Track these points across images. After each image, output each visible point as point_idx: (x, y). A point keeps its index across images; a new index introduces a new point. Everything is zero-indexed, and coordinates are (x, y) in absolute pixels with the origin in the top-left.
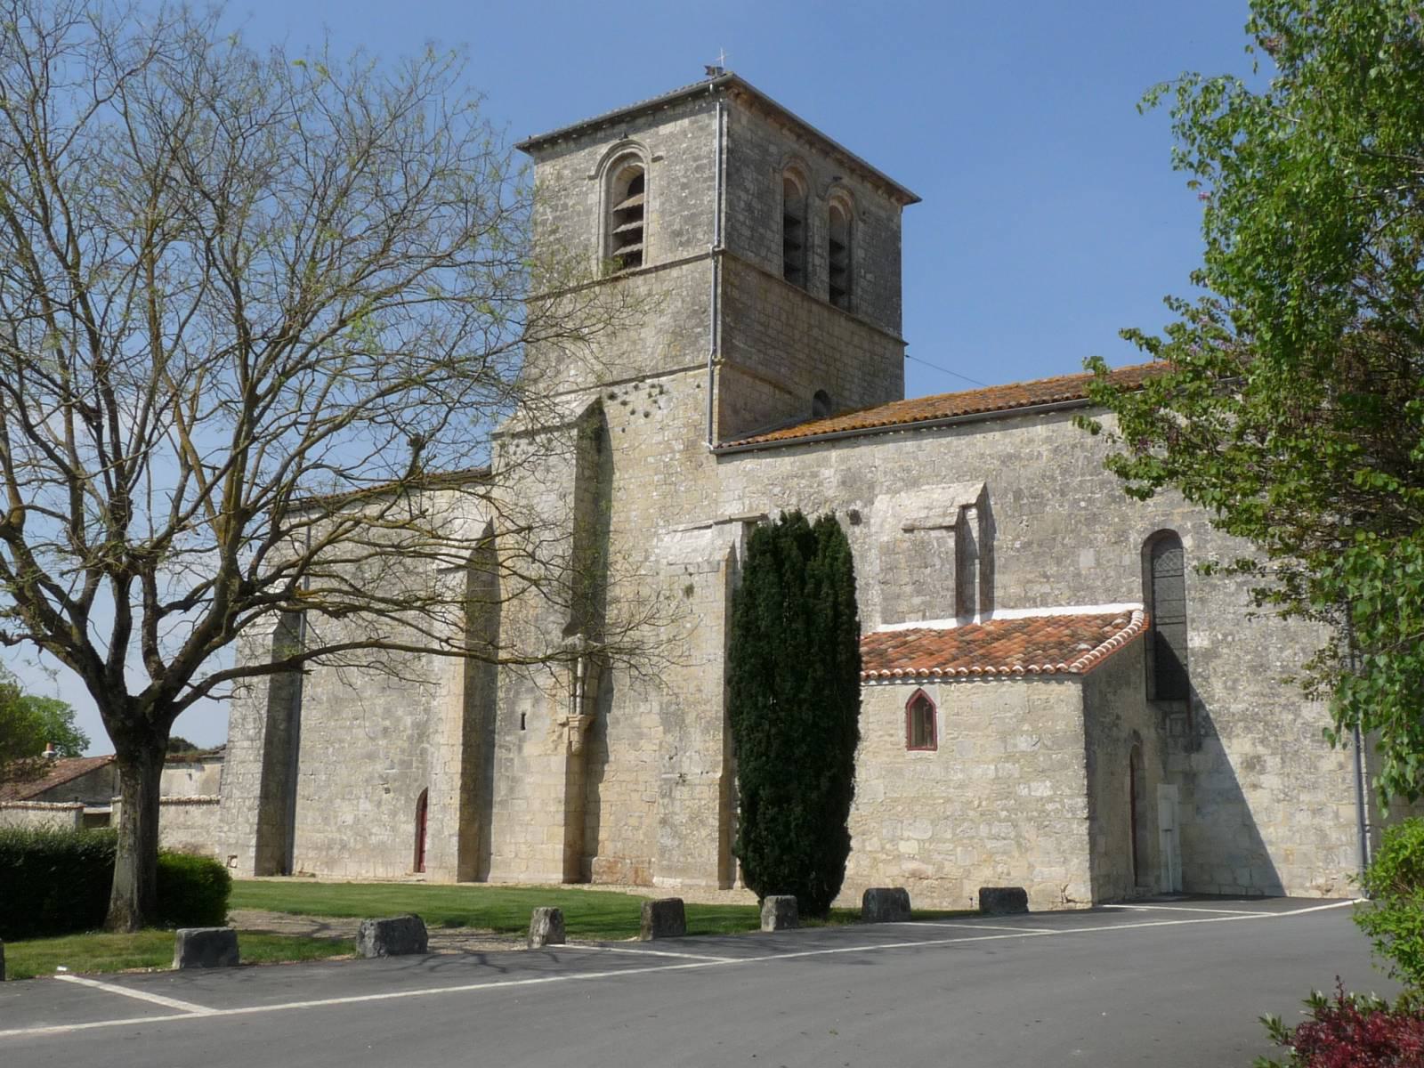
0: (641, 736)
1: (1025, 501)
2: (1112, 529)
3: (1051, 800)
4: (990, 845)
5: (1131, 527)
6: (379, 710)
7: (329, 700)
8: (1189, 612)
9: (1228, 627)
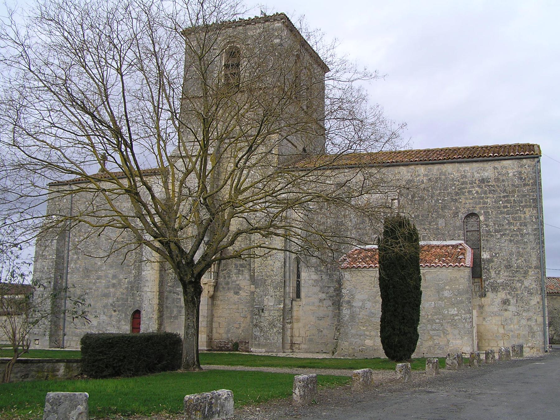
0: (240, 289)
1: (416, 199)
2: (452, 211)
3: (457, 315)
4: (431, 332)
5: (460, 211)
6: (110, 276)
7: (83, 270)
8: (482, 245)
9: (497, 251)
